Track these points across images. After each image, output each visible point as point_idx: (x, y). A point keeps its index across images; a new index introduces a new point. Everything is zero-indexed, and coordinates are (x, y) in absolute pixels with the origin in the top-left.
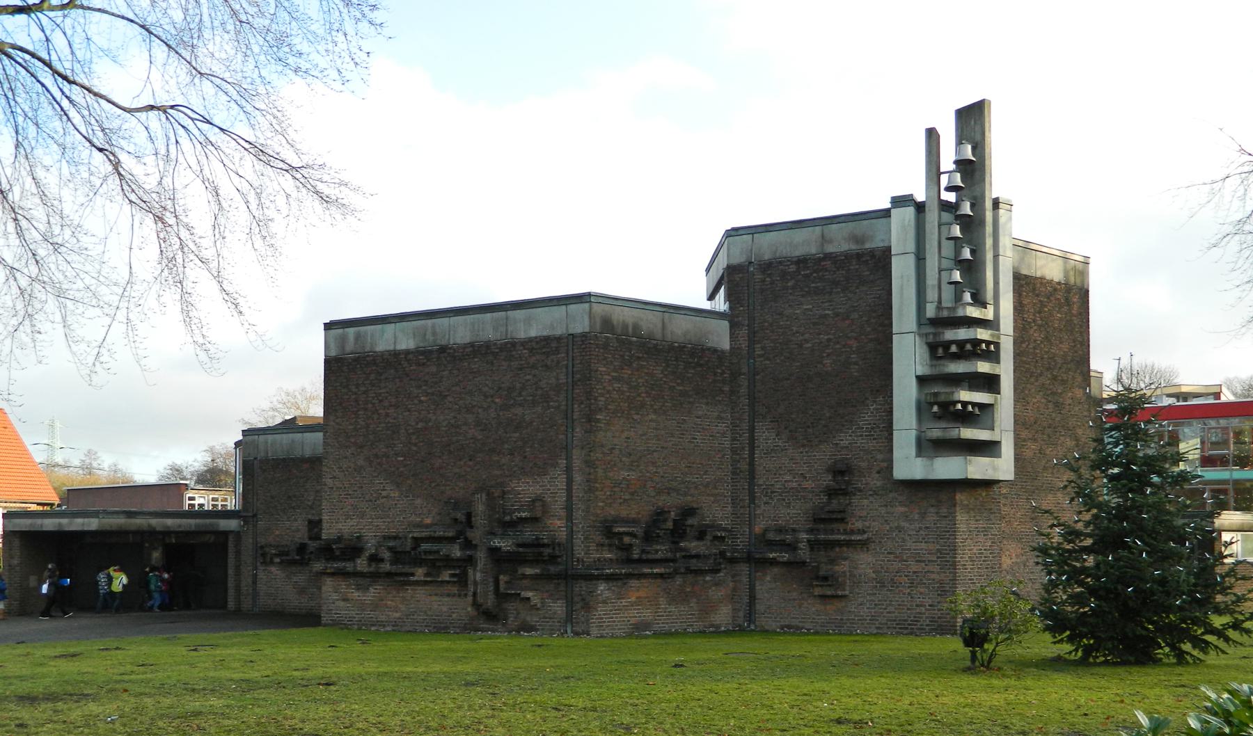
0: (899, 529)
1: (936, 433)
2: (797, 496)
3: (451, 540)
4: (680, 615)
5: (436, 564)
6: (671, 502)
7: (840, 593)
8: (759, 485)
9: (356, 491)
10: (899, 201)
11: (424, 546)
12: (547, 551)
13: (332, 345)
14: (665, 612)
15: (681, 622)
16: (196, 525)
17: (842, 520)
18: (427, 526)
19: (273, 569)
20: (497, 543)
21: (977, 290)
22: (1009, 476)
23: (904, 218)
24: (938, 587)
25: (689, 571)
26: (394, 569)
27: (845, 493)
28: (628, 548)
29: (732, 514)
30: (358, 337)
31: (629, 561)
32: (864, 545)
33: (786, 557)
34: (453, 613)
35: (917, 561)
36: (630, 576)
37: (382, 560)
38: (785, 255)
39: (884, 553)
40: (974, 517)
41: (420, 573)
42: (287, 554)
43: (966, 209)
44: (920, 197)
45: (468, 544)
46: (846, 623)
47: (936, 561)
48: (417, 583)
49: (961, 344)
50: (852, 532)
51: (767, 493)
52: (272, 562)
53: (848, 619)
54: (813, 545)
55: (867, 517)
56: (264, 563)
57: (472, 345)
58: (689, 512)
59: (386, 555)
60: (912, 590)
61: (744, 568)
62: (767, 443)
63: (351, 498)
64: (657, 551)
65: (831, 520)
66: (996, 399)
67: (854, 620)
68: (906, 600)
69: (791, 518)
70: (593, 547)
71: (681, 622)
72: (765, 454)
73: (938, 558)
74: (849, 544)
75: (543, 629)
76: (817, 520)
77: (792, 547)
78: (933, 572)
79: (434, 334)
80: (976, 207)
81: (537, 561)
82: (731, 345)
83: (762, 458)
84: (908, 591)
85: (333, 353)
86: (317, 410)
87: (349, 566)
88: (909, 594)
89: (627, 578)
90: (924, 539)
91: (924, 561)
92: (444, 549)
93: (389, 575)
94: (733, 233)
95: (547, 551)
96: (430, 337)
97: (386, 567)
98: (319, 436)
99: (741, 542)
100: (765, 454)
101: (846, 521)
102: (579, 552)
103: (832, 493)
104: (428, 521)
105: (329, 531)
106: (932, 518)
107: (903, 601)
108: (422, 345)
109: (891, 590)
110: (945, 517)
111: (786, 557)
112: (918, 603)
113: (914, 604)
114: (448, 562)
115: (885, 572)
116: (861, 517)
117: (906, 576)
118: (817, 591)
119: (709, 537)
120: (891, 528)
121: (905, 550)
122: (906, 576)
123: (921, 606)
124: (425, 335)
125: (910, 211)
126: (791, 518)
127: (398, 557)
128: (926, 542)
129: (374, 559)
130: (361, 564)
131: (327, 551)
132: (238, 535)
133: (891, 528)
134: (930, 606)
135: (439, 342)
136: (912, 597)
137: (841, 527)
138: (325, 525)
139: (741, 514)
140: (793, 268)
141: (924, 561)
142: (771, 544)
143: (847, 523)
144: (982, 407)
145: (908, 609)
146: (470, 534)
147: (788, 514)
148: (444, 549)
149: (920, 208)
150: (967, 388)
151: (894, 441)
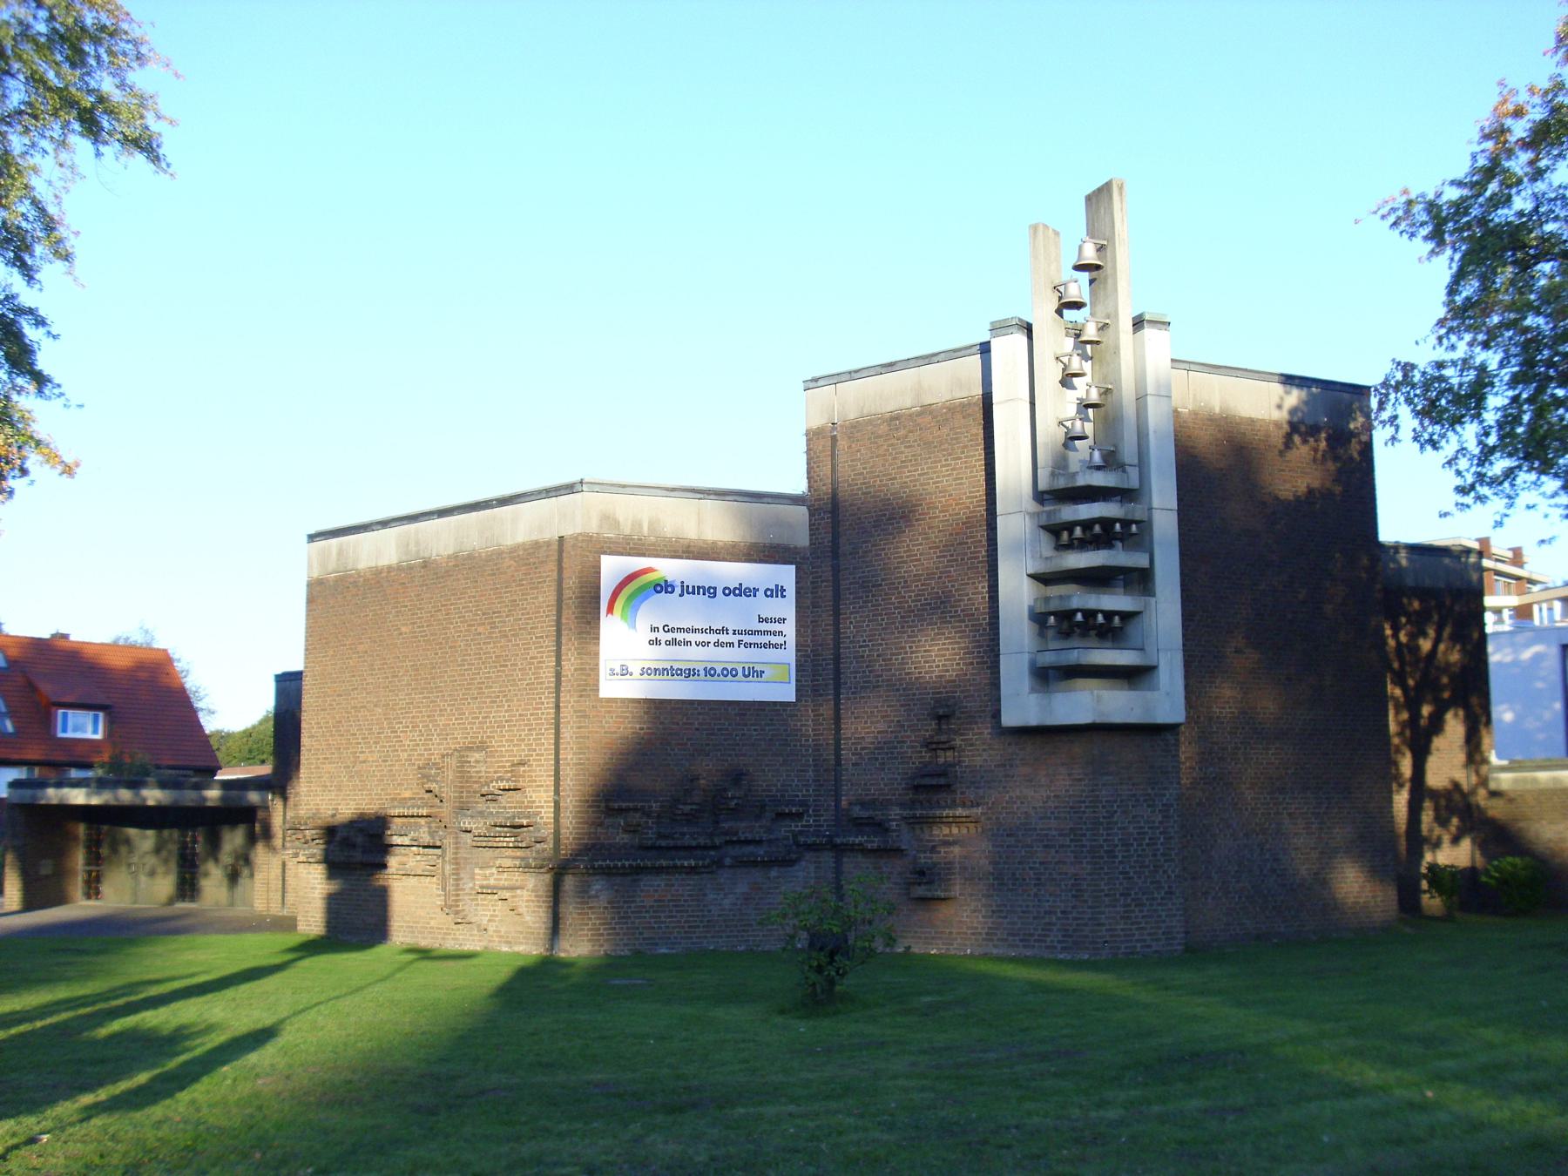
1: (1048, 659)
2: (892, 753)
4: (727, 926)
7: (942, 895)
8: (846, 739)
9: (333, 753)
13: (315, 565)
14: (701, 922)
15: (728, 937)
16: (1516, 781)
21: (1115, 446)
24: (1073, 885)
29: (814, 781)
30: (340, 552)
34: (431, 918)
35: (1046, 846)
36: (638, 870)
37: (354, 846)
38: (873, 412)
39: (1002, 835)
40: (1130, 779)
46: (956, 939)
47: (1069, 846)
51: (856, 749)
53: (959, 933)
55: (980, 782)
57: (455, 556)
60: (1039, 890)
61: (827, 858)
62: (855, 678)
63: (330, 763)
64: (683, 834)
66: (1146, 605)
67: (966, 933)
68: (1031, 904)
69: (885, 785)
71: (728, 937)
72: (853, 693)
73: (1071, 840)
78: (1065, 863)
79: (417, 543)
80: (1111, 330)
82: (811, 540)
83: (849, 699)
84: (1035, 890)
85: (315, 575)
88: (1036, 895)
89: (638, 874)
90: (1053, 813)
91: (1054, 846)
94: (812, 385)
96: (413, 548)
99: (825, 820)
100: (853, 693)
101: (952, 788)
103: (932, 746)
106: (1063, 783)
107: (1027, 906)
108: (404, 558)
109: (1012, 890)
110: (1080, 780)
111: (875, 842)
112: (1048, 909)
113: (1042, 910)
115: (1005, 863)
116: (974, 783)
117: (1031, 868)
120: (1011, 798)
121: (1030, 830)
122: (1031, 868)
123: (1050, 913)
124: (408, 545)
126: (885, 785)
128: (1056, 818)
133: (1011, 798)
134: (1062, 912)
135: (422, 555)
136: (1039, 901)
139: (824, 781)
140: (884, 428)
141: (1054, 846)
142: (860, 824)
143: (954, 792)
144: (1127, 616)
145: (1035, 918)
147: (883, 779)
150: (1122, 590)
151: (1002, 667)
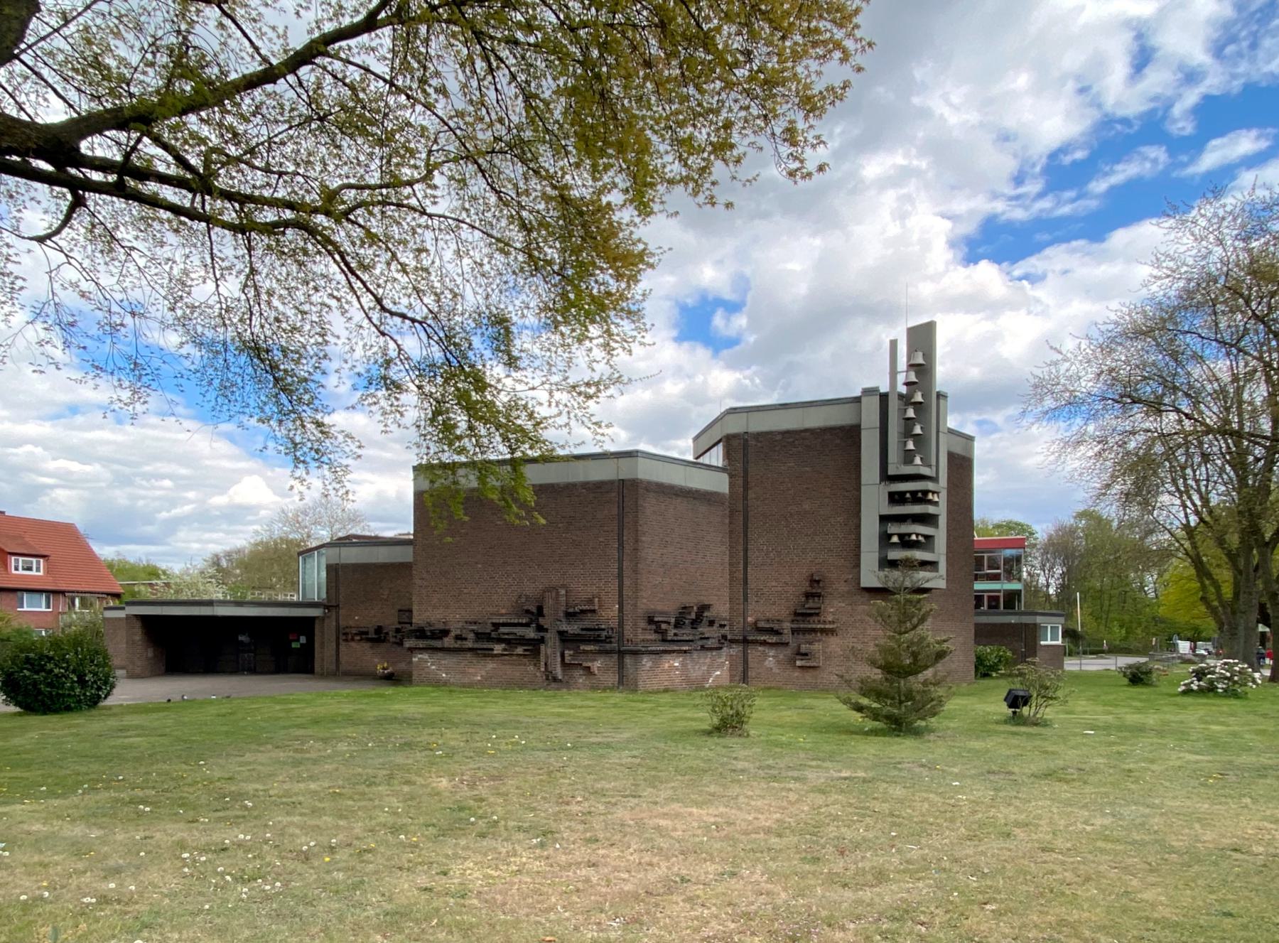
0: (862, 621)
3: (527, 625)
5: (511, 642)
6: (692, 600)
10: (868, 392)
11: (503, 630)
12: (604, 633)
17: (817, 614)
18: (502, 615)
19: (353, 644)
20: (564, 627)
22: (942, 584)
23: (871, 406)
25: (703, 648)
26: (476, 646)
27: (819, 596)
28: (664, 633)
31: (664, 640)
32: (832, 632)
33: (774, 639)
41: (498, 648)
42: (367, 633)
43: (918, 397)
44: (884, 388)
45: (540, 628)
48: (496, 655)
49: (914, 493)
50: (825, 622)
52: (353, 640)
54: (794, 631)
56: (346, 640)
58: (704, 608)
59: (471, 636)
65: (811, 615)
70: (640, 631)
74: (823, 631)
75: (1148, 919)
76: (796, 614)
77: (777, 633)
81: (596, 640)
86: (406, 528)
87: (438, 644)
92: (520, 631)
93: (470, 650)
95: (604, 633)
97: (469, 644)
98: (410, 549)
102: (628, 633)
103: (808, 596)
104: (503, 611)
105: (419, 618)
114: (522, 641)
118: (798, 663)
119: (716, 625)
125: (876, 400)
127: (479, 636)
129: (458, 638)
130: (448, 642)
131: (420, 633)
132: (322, 619)
137: (816, 619)
138: (415, 613)
144: (926, 537)
146: (541, 620)
148: (520, 631)
149: (884, 398)
